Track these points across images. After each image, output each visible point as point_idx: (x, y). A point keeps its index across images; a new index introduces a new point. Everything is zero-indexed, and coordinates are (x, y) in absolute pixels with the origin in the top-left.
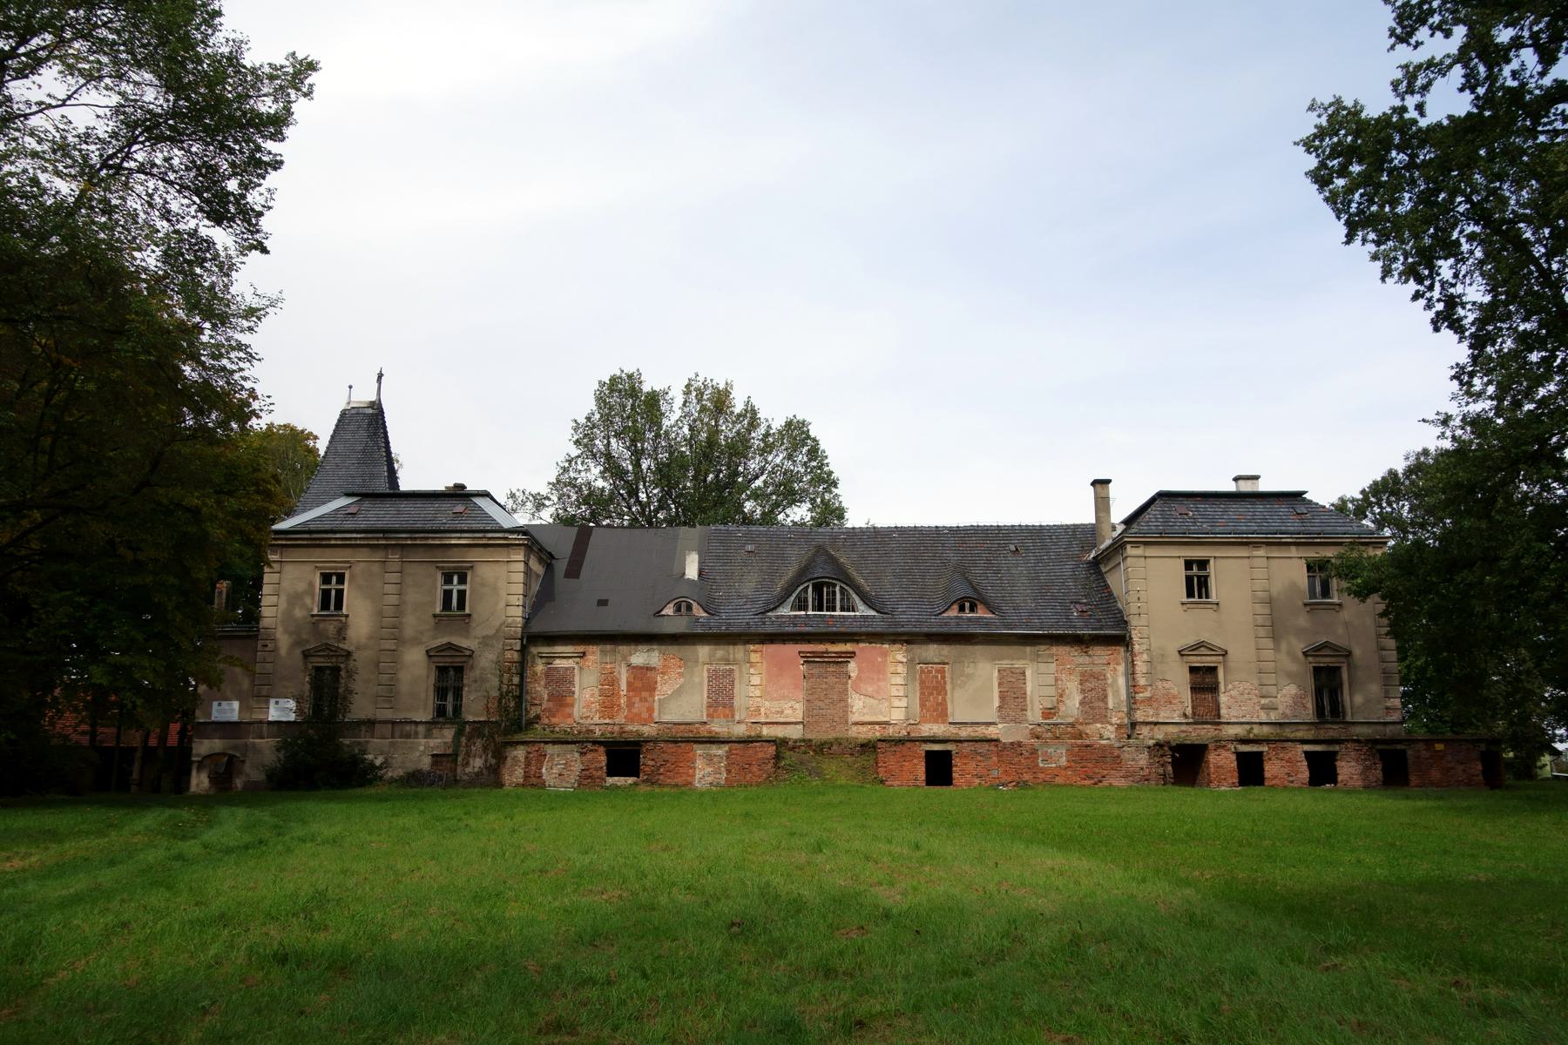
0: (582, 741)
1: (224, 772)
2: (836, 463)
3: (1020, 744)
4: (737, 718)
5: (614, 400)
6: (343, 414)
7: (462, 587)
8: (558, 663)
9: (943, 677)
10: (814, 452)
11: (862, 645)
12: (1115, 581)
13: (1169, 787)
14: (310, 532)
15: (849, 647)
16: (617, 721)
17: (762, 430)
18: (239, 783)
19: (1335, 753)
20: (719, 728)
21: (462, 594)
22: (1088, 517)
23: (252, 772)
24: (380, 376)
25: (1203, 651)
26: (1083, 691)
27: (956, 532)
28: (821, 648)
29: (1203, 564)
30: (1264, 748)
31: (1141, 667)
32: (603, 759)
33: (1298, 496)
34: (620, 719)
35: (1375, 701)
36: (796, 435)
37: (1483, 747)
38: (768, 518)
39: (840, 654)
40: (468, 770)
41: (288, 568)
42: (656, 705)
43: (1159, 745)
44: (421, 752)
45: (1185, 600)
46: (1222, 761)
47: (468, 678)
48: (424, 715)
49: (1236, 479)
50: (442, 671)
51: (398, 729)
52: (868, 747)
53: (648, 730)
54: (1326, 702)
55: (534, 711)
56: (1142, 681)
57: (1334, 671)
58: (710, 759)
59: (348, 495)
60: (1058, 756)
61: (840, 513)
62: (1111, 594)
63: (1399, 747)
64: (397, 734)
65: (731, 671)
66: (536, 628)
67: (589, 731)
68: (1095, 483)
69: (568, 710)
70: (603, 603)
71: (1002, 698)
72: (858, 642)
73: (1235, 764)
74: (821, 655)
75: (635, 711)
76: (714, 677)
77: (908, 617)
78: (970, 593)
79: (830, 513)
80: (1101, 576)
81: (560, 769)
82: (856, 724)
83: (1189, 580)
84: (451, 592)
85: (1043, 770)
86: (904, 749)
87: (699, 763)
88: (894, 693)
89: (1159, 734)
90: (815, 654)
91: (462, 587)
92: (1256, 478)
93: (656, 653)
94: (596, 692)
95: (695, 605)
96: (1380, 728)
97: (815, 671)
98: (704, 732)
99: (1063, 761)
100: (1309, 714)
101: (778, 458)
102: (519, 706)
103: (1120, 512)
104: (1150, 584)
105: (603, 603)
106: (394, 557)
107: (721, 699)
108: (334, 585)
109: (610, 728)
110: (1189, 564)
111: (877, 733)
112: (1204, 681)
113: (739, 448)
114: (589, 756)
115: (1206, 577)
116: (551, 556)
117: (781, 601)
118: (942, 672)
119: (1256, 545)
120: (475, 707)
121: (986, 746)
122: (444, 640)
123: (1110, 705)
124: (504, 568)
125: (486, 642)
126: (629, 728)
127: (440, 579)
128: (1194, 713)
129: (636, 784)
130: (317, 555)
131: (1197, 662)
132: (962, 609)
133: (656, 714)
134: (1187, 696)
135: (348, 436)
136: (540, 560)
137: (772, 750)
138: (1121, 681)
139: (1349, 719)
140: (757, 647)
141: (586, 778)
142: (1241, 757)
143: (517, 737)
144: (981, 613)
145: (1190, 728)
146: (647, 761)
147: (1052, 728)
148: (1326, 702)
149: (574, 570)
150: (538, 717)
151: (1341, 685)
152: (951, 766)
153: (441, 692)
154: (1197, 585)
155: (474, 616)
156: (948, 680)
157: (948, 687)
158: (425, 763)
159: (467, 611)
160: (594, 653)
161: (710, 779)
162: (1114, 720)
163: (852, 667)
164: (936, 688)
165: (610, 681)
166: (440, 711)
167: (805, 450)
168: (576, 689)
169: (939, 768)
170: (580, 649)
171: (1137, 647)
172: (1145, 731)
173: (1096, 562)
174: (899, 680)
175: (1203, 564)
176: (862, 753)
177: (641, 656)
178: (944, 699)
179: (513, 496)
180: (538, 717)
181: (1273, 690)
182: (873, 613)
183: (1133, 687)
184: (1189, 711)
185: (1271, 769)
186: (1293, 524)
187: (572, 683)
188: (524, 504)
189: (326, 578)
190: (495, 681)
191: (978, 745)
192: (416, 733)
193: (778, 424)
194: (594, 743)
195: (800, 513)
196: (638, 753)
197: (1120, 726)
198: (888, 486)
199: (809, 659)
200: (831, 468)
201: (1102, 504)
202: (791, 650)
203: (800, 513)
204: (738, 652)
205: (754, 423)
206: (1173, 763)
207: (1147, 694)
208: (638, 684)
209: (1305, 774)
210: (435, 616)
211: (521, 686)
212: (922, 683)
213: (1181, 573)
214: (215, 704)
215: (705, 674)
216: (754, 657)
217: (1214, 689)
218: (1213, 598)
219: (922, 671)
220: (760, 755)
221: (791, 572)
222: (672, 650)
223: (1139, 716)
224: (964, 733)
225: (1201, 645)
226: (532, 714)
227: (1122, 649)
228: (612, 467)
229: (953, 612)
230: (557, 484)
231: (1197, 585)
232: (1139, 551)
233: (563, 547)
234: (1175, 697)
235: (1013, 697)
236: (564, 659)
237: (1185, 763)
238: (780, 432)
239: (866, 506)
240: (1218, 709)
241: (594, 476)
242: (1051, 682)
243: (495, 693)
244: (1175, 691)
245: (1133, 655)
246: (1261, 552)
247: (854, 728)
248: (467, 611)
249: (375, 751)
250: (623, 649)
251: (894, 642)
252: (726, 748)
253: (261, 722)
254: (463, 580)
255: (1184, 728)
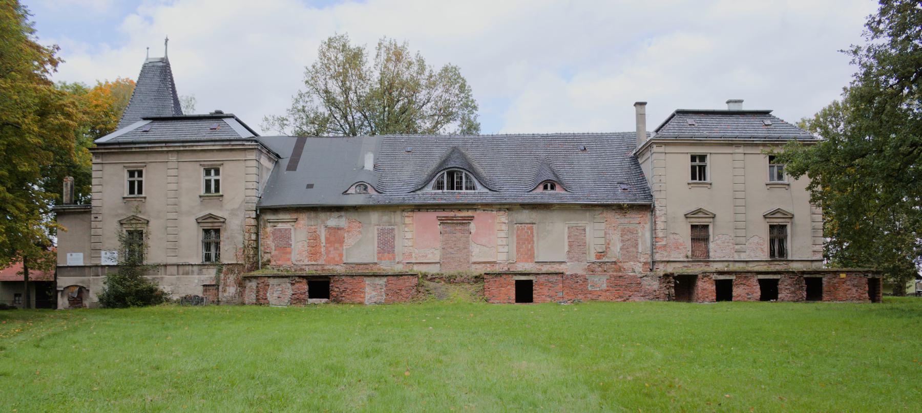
0: (294, 278)
1: (78, 298)
2: (476, 95)
3: (576, 276)
4: (397, 260)
5: (332, 54)
6: (144, 67)
7: (217, 178)
8: (280, 226)
9: (532, 233)
10: (462, 88)
11: (478, 212)
12: (646, 167)
13: (671, 303)
14: (119, 144)
15: (470, 213)
16: (319, 263)
17: (427, 73)
18: (87, 303)
19: (778, 280)
20: (386, 266)
21: (217, 182)
22: (633, 129)
23: (93, 297)
24: (167, 40)
25: (700, 215)
26: (622, 241)
27: (545, 137)
28: (451, 214)
29: (703, 158)
30: (733, 277)
31: (660, 225)
32: (306, 287)
33: (766, 113)
34: (321, 261)
35: (808, 246)
36: (451, 77)
37: (870, 276)
38: (433, 130)
39: (464, 218)
40: (225, 295)
41: (107, 167)
42: (344, 252)
43: (666, 276)
44: (193, 284)
45: (690, 181)
46: (706, 287)
47: (224, 236)
48: (198, 259)
49: (728, 102)
50: (207, 231)
51: (181, 268)
52: (478, 279)
53: (340, 269)
54: (776, 247)
55: (266, 257)
56: (660, 234)
57: (783, 227)
58: (375, 287)
59: (145, 119)
60: (601, 282)
61: (477, 128)
62: (644, 178)
63: (818, 276)
64: (181, 272)
65: (393, 229)
66: (266, 204)
67: (301, 270)
68: (637, 104)
69: (288, 256)
70: (310, 186)
71: (570, 246)
72: (476, 209)
73: (714, 287)
74: (452, 219)
75: (331, 256)
76: (382, 233)
77: (510, 194)
78: (554, 179)
79: (471, 128)
80: (637, 165)
81: (279, 293)
82: (475, 263)
83: (693, 168)
84: (210, 180)
85: (590, 293)
86: (502, 280)
87: (368, 289)
88: (499, 242)
89: (670, 269)
90: (447, 218)
91: (208, 178)
92: (741, 101)
93: (344, 219)
94: (306, 245)
95: (369, 187)
96: (809, 263)
97: (448, 229)
98: (375, 270)
99: (604, 287)
100: (765, 256)
101: (439, 91)
102: (256, 254)
103: (652, 125)
104: (668, 172)
105: (310, 186)
106: (173, 158)
107: (386, 245)
108: (136, 178)
109: (315, 267)
110: (693, 158)
111: (489, 269)
112: (700, 234)
113: (414, 87)
114: (297, 285)
115: (704, 167)
116: (278, 156)
117: (426, 183)
118: (532, 229)
119: (738, 145)
120: (228, 255)
121: (555, 277)
122: (207, 212)
123: (640, 250)
124: (243, 163)
125: (233, 213)
126: (326, 268)
127: (203, 173)
128: (693, 255)
129: (327, 303)
130: (124, 159)
131: (696, 222)
132: (545, 188)
133: (344, 258)
134: (689, 243)
135: (148, 81)
136: (270, 159)
137: (77, 289)
138: (648, 235)
139: (789, 258)
140: (410, 214)
141: (296, 300)
142: (718, 283)
143: (255, 273)
144: (558, 190)
145: (690, 264)
146: (335, 289)
147: (602, 263)
148: (776, 247)
149: (292, 166)
150: (269, 261)
151: (786, 237)
152: (532, 290)
153: (207, 246)
154: (698, 172)
155: (225, 196)
156: (535, 234)
157: (535, 239)
158: (199, 292)
159: (221, 193)
160: (304, 220)
161: (374, 300)
162: (642, 260)
163: (472, 226)
164: (527, 240)
165: (314, 238)
166: (208, 258)
167: (457, 86)
168: (293, 243)
169: (524, 292)
170: (294, 216)
171: (658, 212)
172: (661, 266)
173: (635, 158)
174: (503, 235)
175: (703, 158)
176: (476, 282)
177: (333, 221)
178: (532, 247)
179: (266, 119)
180: (269, 261)
181: (743, 240)
182: (487, 191)
183: (654, 238)
184: (690, 254)
185: (736, 291)
186: (762, 132)
187: (289, 238)
188: (274, 125)
189: (131, 174)
190: (241, 238)
191: (550, 276)
192: (193, 272)
193: (437, 70)
194: (300, 277)
195: (452, 128)
196: (328, 283)
197: (645, 263)
198: (519, 107)
199: (443, 221)
200: (474, 97)
201: (641, 118)
202: (432, 216)
203: (452, 128)
204: (397, 217)
205: (422, 67)
206: (676, 287)
207: (664, 243)
208: (332, 239)
209: (758, 294)
210: (200, 197)
211: (257, 240)
212: (518, 236)
213: (689, 164)
214: (68, 255)
215: (376, 232)
216: (407, 220)
217: (706, 239)
218: (708, 180)
219: (518, 229)
220: (407, 284)
221: (433, 165)
222: (354, 216)
223: (658, 257)
224: (545, 269)
225: (699, 211)
226: (265, 259)
227: (649, 214)
228: (330, 101)
229: (540, 189)
230: (295, 110)
231: (698, 172)
232: (662, 149)
233: (286, 153)
234: (681, 245)
235: (577, 244)
236: (283, 222)
237: (683, 287)
238: (440, 74)
239: (494, 122)
240: (708, 252)
241: (318, 105)
242: (601, 234)
243: (242, 246)
244: (681, 241)
245: (656, 217)
246: (741, 150)
247: (474, 266)
248: (221, 193)
249: (166, 284)
250: (322, 216)
251: (500, 210)
252: (385, 279)
253: (97, 266)
254: (217, 172)
255: (686, 264)
